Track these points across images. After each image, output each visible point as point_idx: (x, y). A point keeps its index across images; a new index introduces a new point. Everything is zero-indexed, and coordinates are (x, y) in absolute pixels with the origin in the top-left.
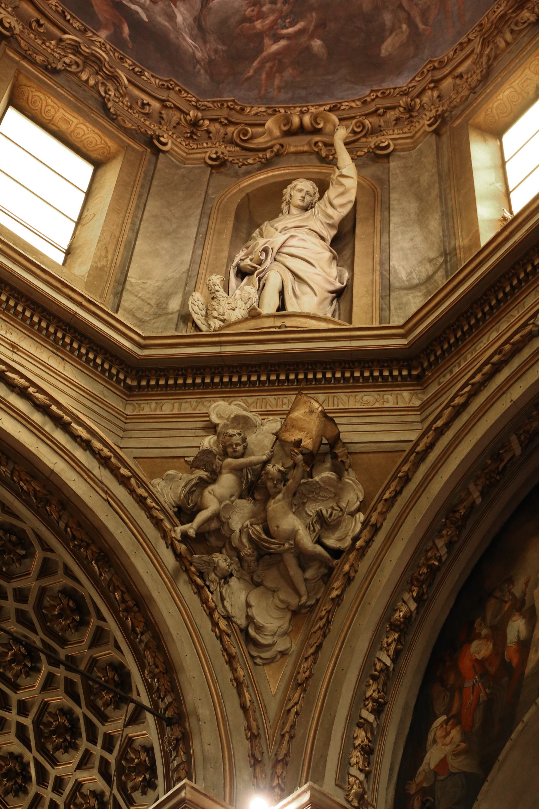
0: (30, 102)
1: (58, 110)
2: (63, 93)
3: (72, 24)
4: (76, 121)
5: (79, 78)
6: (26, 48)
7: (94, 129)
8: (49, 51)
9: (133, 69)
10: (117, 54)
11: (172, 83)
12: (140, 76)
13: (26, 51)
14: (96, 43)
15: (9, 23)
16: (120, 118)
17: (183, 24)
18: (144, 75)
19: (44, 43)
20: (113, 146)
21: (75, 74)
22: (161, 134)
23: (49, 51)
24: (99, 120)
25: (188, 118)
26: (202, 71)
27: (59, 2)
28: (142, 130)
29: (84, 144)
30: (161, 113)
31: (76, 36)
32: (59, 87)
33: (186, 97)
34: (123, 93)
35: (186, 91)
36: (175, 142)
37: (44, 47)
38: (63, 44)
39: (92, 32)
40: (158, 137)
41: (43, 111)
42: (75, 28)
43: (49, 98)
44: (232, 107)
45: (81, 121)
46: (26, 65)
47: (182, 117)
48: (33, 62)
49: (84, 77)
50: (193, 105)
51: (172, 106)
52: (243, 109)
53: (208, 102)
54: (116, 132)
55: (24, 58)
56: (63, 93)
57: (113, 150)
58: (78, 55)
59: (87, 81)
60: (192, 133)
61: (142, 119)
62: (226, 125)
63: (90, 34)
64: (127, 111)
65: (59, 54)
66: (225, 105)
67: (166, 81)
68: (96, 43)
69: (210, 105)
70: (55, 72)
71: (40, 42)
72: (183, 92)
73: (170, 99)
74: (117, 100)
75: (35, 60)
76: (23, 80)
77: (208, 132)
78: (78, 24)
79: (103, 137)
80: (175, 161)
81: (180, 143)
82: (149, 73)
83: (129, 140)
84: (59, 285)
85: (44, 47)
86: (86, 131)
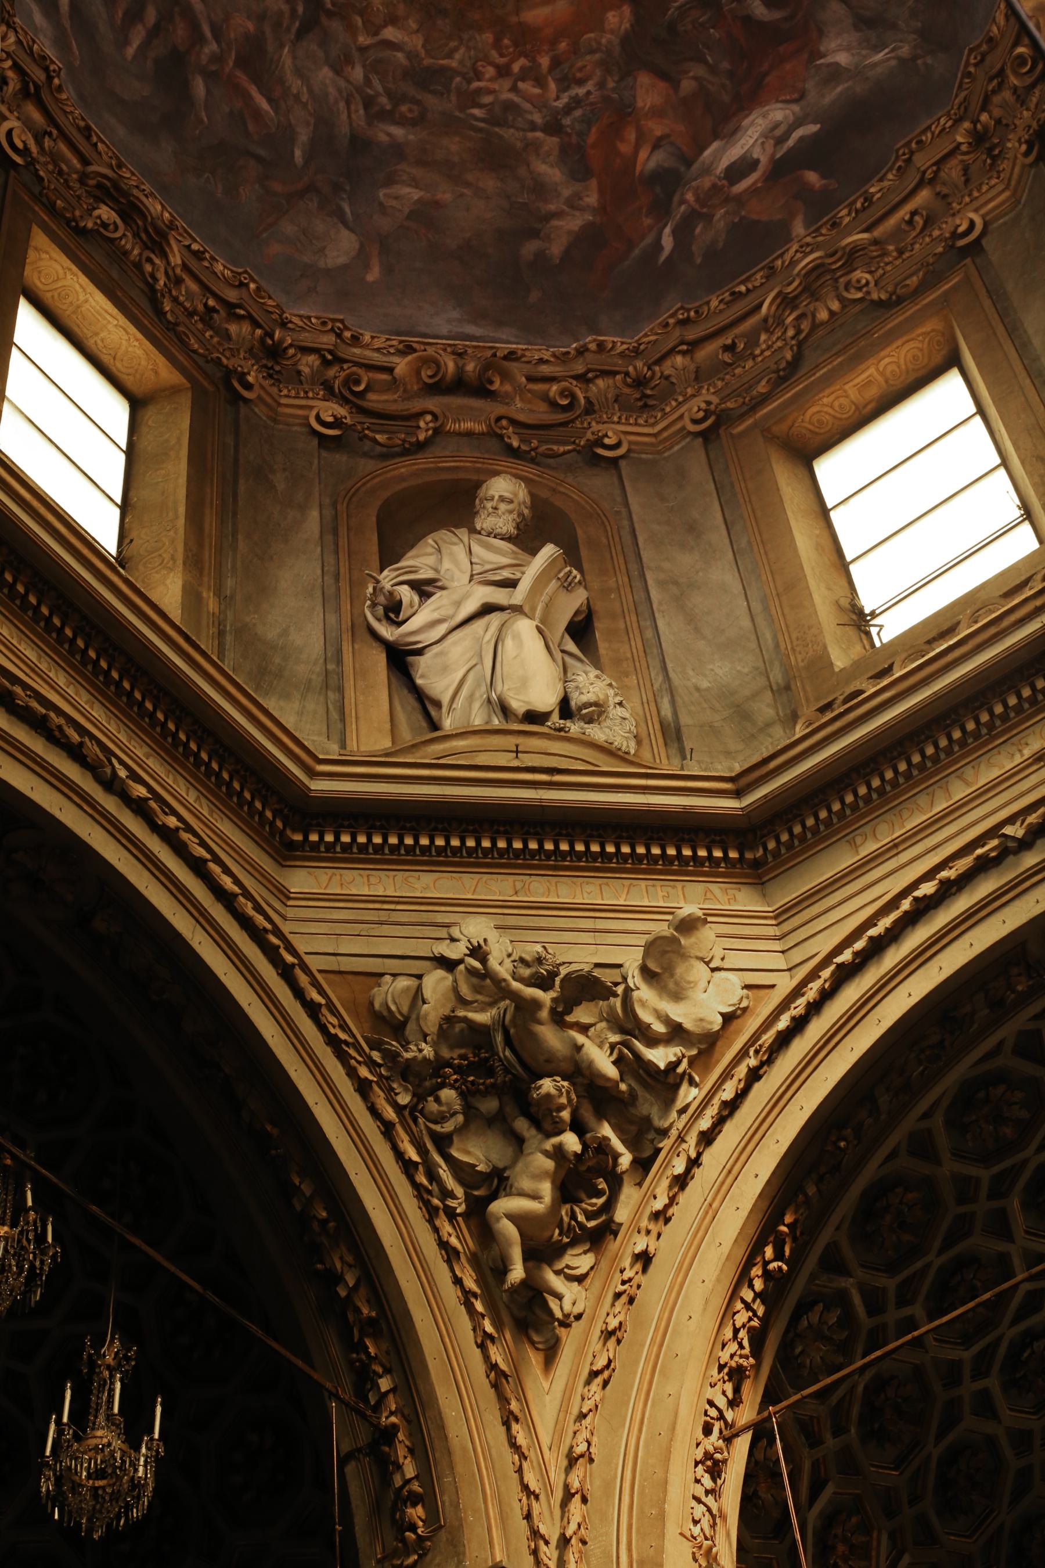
0: (817, 430)
1: (845, 391)
2: (825, 370)
3: (755, 287)
4: (872, 370)
5: (822, 323)
6: (741, 400)
7: (894, 346)
8: (767, 353)
9: (857, 211)
10: (824, 231)
11: (901, 152)
12: (871, 203)
13: (744, 403)
14: (795, 258)
15: (699, 410)
16: (898, 291)
17: (853, 55)
18: (873, 195)
19: (754, 357)
20: (932, 325)
21: (815, 326)
22: (952, 229)
23: (767, 353)
24: (889, 326)
25: (964, 148)
26: (929, 60)
27: (718, 293)
28: (931, 261)
29: (913, 370)
30: (938, 194)
31: (772, 290)
32: (814, 374)
33: (933, 133)
34: (879, 253)
35: (924, 132)
36: (976, 204)
37: (760, 359)
38: (771, 320)
39: (777, 258)
40: (955, 235)
41: (839, 415)
42: (762, 284)
43: (820, 399)
44: (979, 58)
45: (875, 361)
46: (765, 411)
47: (960, 157)
48: (764, 399)
49: (823, 315)
50: (950, 127)
51: (934, 168)
52: (990, 40)
53: (957, 96)
54: (918, 307)
55: (753, 408)
56: (825, 370)
57: (940, 326)
58: (798, 302)
59: (832, 313)
60: (990, 150)
61: (927, 239)
62: (1000, 85)
63: (779, 262)
64: (904, 260)
65: (778, 339)
66: (972, 69)
67: (897, 158)
68: (795, 258)
69: (963, 94)
70: (794, 365)
71: (750, 364)
72: (924, 138)
73: (923, 169)
74: (881, 271)
75: (762, 394)
76: (780, 429)
77: (998, 122)
78: (758, 276)
79: (913, 336)
80: (1006, 218)
81: (991, 187)
82: (873, 185)
83: (939, 289)
84: (993, 630)
85: (760, 359)
86: (894, 359)
